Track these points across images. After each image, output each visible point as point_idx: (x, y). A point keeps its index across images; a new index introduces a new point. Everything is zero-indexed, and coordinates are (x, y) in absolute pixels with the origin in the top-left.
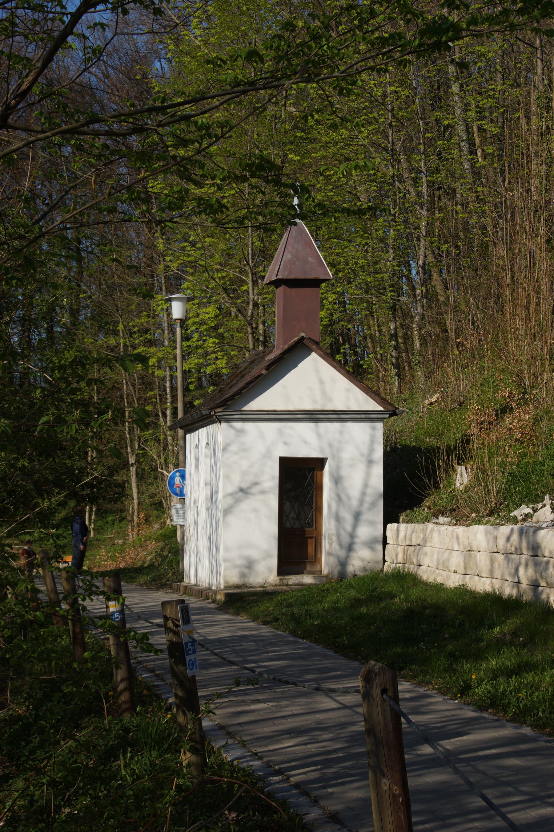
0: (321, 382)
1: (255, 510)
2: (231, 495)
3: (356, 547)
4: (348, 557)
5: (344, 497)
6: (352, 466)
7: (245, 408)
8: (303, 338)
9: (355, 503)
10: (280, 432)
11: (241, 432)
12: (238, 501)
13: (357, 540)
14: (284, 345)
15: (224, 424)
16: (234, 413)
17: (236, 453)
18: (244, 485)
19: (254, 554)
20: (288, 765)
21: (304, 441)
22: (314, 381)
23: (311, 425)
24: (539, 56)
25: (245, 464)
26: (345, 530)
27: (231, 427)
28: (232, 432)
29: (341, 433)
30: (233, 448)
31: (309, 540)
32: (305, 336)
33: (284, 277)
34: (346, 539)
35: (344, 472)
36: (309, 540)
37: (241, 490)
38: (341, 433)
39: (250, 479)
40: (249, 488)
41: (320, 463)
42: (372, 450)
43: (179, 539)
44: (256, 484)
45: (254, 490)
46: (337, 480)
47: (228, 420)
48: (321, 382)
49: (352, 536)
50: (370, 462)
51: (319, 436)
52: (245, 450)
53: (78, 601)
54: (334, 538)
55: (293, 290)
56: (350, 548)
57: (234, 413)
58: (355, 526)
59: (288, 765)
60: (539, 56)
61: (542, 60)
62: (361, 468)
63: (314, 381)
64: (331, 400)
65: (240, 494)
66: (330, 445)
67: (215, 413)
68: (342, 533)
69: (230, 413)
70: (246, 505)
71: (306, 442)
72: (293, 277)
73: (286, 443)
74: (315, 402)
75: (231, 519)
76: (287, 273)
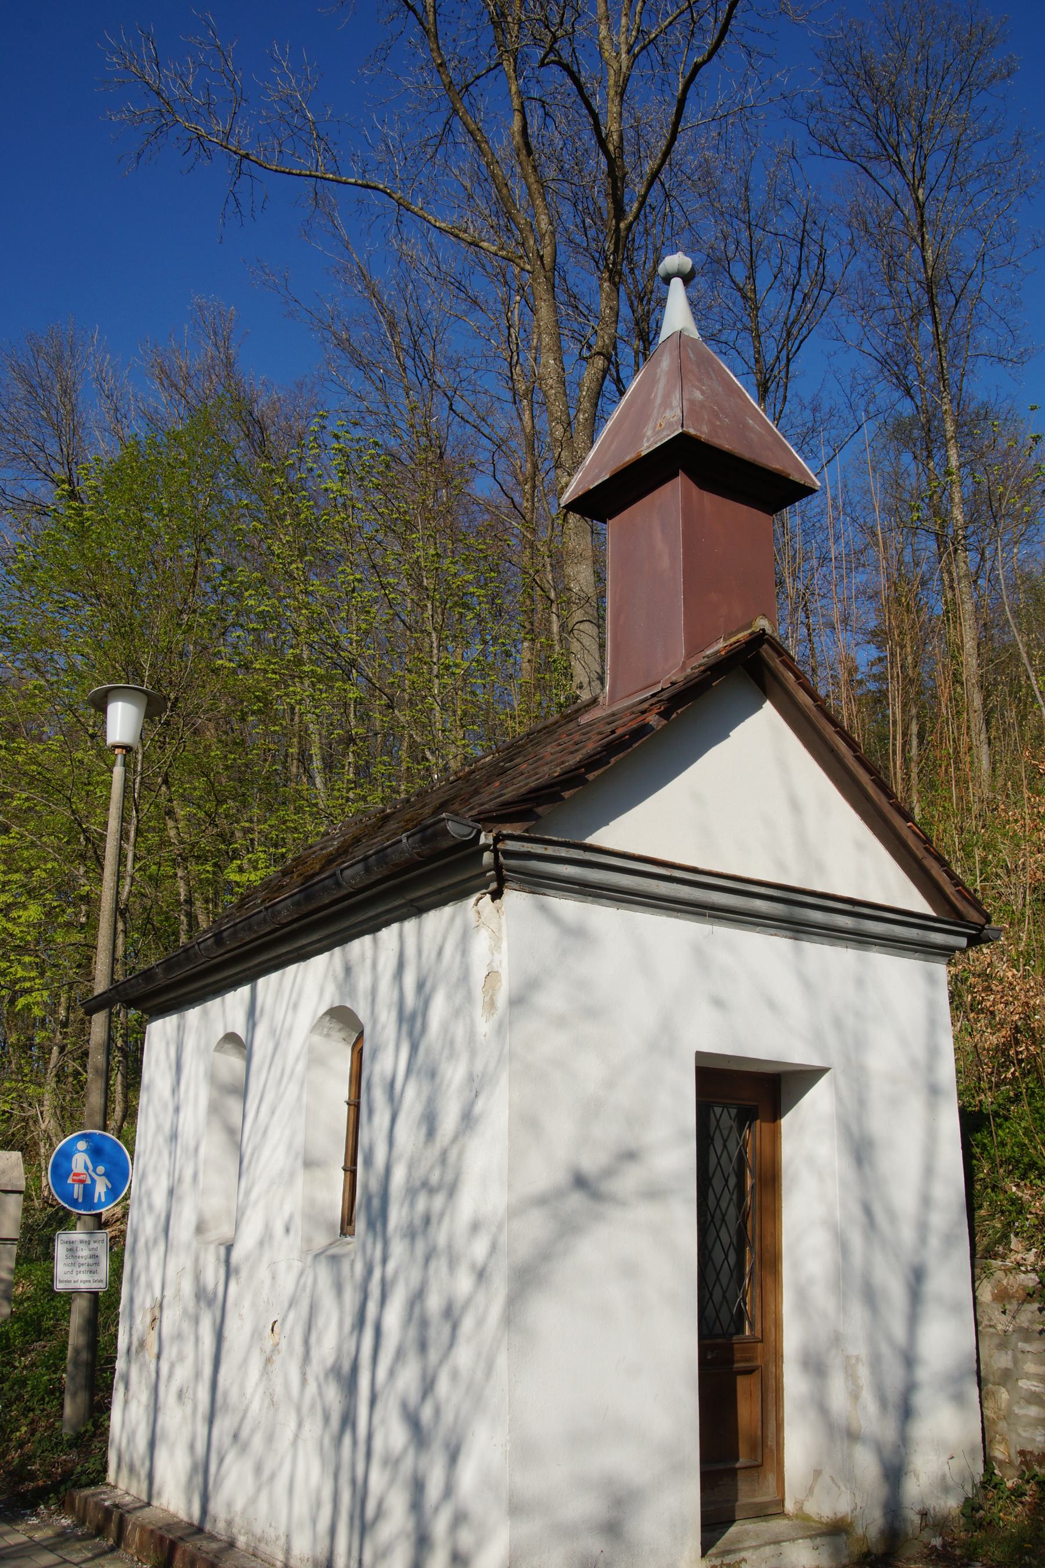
0: (795, 806)
1: (629, 1270)
2: (542, 1201)
3: (922, 1399)
4: (904, 1441)
5: (880, 1217)
10: (700, 956)
11: (577, 934)
12: (568, 1229)
13: (923, 1374)
14: (689, 655)
15: (514, 898)
16: (563, 852)
17: (561, 1022)
18: (590, 1163)
19: (627, 1462)
21: (764, 996)
22: (752, 795)
24: (554, 610)
25: (591, 1069)
26: (890, 1339)
27: (543, 909)
28: (549, 932)
29: (860, 983)
30: (552, 999)
32: (769, 631)
34: (894, 1375)
35: (878, 1123)
37: (580, 1182)
38: (860, 983)
39: (609, 1133)
40: (609, 1173)
41: (804, 1078)
42: (933, 1052)
44: (630, 1156)
45: (628, 1181)
47: (537, 883)
48: (795, 806)
49: (909, 1360)
50: (934, 1091)
51: (807, 985)
52: (591, 1013)
54: (863, 1373)
56: (906, 1412)
57: (563, 852)
58: (913, 1319)
60: (554, 610)
61: (558, 616)
62: (915, 1105)
64: (820, 868)
65: (576, 1200)
66: (838, 1024)
68: (885, 1350)
69: (551, 851)
70: (596, 1249)
71: (772, 1005)
73: (718, 1003)
74: (781, 866)
75: (546, 1312)
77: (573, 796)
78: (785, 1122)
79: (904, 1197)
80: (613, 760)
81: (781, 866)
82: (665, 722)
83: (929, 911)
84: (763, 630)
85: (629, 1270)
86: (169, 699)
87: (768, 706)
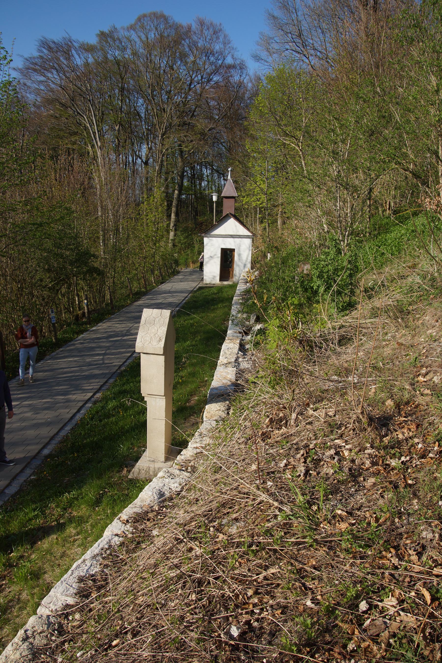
1: (215, 262)
9: (244, 261)
19: (215, 275)
20: (15, 393)
21: (229, 244)
22: (231, 226)
37: (211, 257)
44: (215, 255)
46: (239, 255)
63: (231, 226)
70: (212, 261)
85: (215, 262)
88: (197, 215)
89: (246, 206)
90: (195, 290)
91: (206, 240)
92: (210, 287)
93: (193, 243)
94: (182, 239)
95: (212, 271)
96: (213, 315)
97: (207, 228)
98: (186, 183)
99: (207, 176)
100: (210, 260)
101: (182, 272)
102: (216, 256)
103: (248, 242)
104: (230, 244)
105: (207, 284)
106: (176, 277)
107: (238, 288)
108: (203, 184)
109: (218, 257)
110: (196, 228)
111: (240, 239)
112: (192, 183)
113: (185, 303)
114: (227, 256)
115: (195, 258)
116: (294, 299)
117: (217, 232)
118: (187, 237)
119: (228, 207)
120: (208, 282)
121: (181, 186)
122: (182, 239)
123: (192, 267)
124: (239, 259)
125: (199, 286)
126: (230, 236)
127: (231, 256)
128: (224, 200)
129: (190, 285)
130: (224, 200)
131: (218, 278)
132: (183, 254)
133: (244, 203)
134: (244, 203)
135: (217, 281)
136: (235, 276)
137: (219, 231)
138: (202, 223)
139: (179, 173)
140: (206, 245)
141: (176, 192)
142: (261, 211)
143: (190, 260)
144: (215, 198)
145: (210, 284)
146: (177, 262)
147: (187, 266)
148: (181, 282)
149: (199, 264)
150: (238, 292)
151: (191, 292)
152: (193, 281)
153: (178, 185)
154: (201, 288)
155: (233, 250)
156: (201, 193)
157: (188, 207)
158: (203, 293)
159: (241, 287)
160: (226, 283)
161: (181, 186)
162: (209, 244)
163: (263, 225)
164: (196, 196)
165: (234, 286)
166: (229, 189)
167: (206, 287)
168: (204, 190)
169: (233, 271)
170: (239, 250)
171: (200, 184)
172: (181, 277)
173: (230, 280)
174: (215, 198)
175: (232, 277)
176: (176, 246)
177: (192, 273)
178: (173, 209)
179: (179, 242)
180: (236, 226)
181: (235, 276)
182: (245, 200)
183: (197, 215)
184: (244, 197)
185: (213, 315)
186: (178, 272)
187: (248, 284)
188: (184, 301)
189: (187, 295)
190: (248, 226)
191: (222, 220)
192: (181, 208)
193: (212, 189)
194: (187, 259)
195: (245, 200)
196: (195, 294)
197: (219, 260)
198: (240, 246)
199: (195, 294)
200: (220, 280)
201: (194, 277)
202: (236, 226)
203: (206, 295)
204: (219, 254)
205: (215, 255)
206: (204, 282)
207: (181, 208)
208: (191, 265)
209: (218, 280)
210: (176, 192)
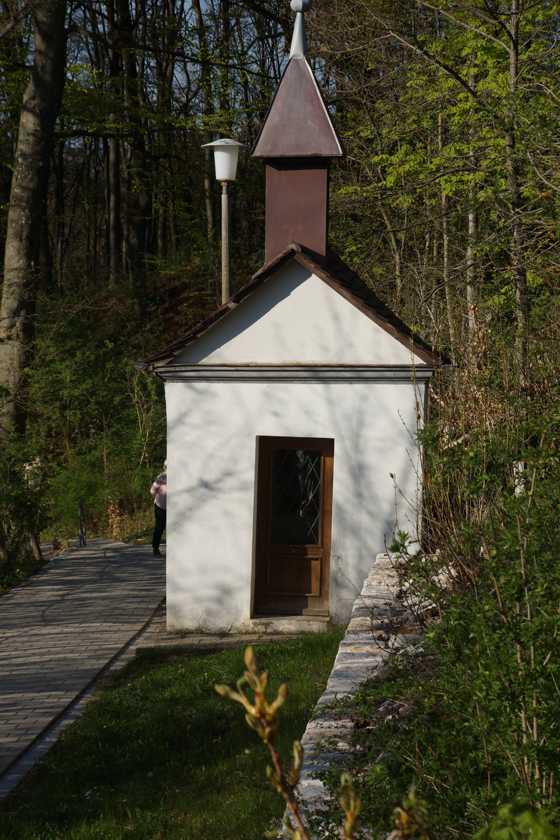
1: (227, 514)
6: (382, 451)
7: (205, 361)
8: (292, 252)
9: (386, 507)
10: (267, 395)
18: (209, 477)
19: (228, 579)
20: (9, 708)
21: (302, 412)
22: (312, 318)
23: (318, 387)
31: (313, 562)
33: (265, 155)
35: (371, 458)
36: (313, 562)
37: (205, 485)
40: (218, 481)
43: (36, 556)
44: (228, 474)
46: (359, 472)
51: (330, 402)
53: (391, 831)
55: (283, 173)
57: (183, 369)
59: (9, 708)
63: (312, 318)
65: (203, 490)
67: (154, 368)
69: (177, 369)
70: (212, 508)
72: (278, 153)
73: (276, 414)
74: (325, 349)
76: (269, 147)
77: (201, 336)
78: (166, 463)
79: (385, 490)
80: (209, 327)
81: (325, 349)
82: (236, 305)
83: (418, 361)
84: (292, 249)
85: (227, 514)
86: (193, 39)
87: (313, 275)
88: (153, 249)
89: (405, 202)
90: (118, 665)
91: (175, 394)
92: (209, 650)
93: (126, 403)
94: (67, 376)
95: (209, 560)
96: (196, 822)
97: (186, 323)
98: (80, 69)
99: (201, 30)
100: (202, 500)
101: (59, 564)
102: (230, 482)
103: (399, 403)
104: (308, 413)
105: (183, 633)
106: (20, 595)
107: (338, 666)
108: (179, 77)
109: (243, 488)
110: (145, 315)
111: (360, 387)
112: (115, 69)
113: (54, 748)
114: (292, 476)
115: (136, 485)
116: (525, 818)
117: (240, 348)
118: (91, 369)
119: (295, 213)
120: (189, 624)
121: (53, 92)
122: (67, 376)
123: (114, 538)
124: (359, 495)
125: (142, 643)
126: (306, 372)
127: (314, 478)
128: (272, 175)
129: (93, 640)
130: (272, 175)
131: (243, 600)
132: (73, 463)
133: (390, 181)
134: (390, 181)
135: (239, 611)
136: (339, 585)
137: (247, 346)
138: (174, 292)
139: (41, 16)
140: (180, 421)
141: (28, 121)
142: (486, 226)
143: (109, 495)
144: (224, 166)
145: (200, 632)
146: (30, 513)
147: (90, 521)
148: (46, 621)
149: (149, 520)
150: (337, 689)
151: (98, 679)
152: (113, 615)
153: (38, 82)
154: (150, 658)
155: (325, 446)
156: (167, 129)
157: (99, 201)
158: (159, 686)
159: (358, 658)
160: (286, 625)
161: (53, 92)
162: (195, 418)
163: (497, 300)
164: (138, 145)
165: (321, 648)
166: (298, 119)
167: (178, 651)
168: (185, 109)
169: (324, 562)
170: (357, 449)
171: (164, 77)
172: (47, 593)
173: (313, 607)
174: (224, 166)
175: (322, 595)
176: (35, 417)
177: (110, 569)
178: (12, 215)
179: (53, 396)
180: (336, 318)
181: (339, 585)
182: (402, 163)
183: (153, 249)
184: (392, 150)
185: (196, 822)
186: (37, 566)
187: (395, 641)
188: (51, 739)
189: (67, 700)
190: (405, 313)
191: (260, 288)
192: (60, 210)
193: (225, 105)
194: (92, 488)
195: (402, 163)
196: (115, 695)
197: (249, 498)
198: (361, 423)
199: (115, 695)
200: (256, 613)
201: (118, 591)
202: (336, 318)
203: (173, 700)
204: (248, 472)
205: (228, 474)
206: (170, 620)
207: (60, 210)
208: (114, 520)
209: (246, 611)
210: (28, 121)
